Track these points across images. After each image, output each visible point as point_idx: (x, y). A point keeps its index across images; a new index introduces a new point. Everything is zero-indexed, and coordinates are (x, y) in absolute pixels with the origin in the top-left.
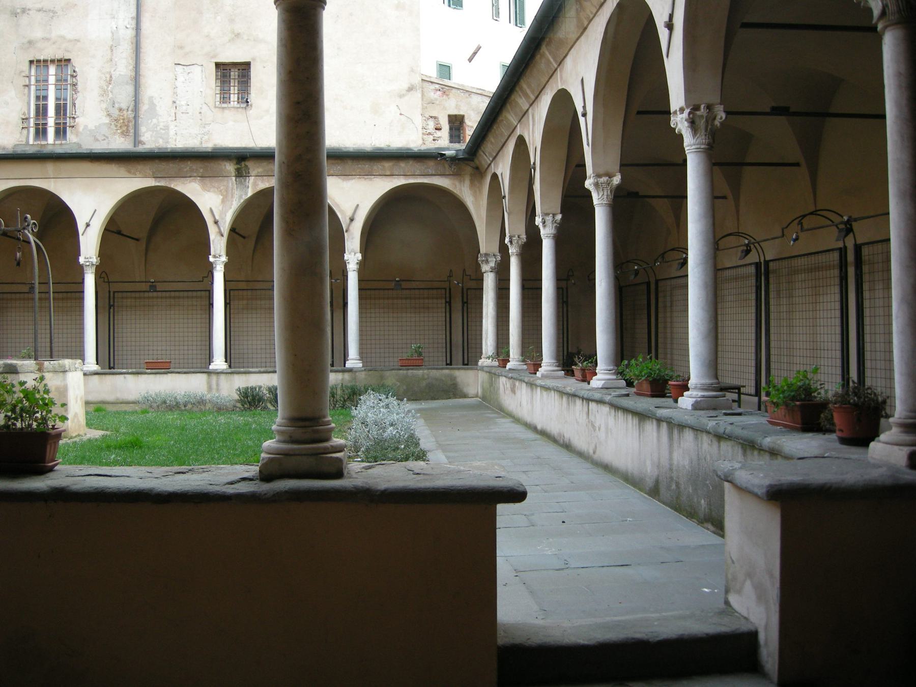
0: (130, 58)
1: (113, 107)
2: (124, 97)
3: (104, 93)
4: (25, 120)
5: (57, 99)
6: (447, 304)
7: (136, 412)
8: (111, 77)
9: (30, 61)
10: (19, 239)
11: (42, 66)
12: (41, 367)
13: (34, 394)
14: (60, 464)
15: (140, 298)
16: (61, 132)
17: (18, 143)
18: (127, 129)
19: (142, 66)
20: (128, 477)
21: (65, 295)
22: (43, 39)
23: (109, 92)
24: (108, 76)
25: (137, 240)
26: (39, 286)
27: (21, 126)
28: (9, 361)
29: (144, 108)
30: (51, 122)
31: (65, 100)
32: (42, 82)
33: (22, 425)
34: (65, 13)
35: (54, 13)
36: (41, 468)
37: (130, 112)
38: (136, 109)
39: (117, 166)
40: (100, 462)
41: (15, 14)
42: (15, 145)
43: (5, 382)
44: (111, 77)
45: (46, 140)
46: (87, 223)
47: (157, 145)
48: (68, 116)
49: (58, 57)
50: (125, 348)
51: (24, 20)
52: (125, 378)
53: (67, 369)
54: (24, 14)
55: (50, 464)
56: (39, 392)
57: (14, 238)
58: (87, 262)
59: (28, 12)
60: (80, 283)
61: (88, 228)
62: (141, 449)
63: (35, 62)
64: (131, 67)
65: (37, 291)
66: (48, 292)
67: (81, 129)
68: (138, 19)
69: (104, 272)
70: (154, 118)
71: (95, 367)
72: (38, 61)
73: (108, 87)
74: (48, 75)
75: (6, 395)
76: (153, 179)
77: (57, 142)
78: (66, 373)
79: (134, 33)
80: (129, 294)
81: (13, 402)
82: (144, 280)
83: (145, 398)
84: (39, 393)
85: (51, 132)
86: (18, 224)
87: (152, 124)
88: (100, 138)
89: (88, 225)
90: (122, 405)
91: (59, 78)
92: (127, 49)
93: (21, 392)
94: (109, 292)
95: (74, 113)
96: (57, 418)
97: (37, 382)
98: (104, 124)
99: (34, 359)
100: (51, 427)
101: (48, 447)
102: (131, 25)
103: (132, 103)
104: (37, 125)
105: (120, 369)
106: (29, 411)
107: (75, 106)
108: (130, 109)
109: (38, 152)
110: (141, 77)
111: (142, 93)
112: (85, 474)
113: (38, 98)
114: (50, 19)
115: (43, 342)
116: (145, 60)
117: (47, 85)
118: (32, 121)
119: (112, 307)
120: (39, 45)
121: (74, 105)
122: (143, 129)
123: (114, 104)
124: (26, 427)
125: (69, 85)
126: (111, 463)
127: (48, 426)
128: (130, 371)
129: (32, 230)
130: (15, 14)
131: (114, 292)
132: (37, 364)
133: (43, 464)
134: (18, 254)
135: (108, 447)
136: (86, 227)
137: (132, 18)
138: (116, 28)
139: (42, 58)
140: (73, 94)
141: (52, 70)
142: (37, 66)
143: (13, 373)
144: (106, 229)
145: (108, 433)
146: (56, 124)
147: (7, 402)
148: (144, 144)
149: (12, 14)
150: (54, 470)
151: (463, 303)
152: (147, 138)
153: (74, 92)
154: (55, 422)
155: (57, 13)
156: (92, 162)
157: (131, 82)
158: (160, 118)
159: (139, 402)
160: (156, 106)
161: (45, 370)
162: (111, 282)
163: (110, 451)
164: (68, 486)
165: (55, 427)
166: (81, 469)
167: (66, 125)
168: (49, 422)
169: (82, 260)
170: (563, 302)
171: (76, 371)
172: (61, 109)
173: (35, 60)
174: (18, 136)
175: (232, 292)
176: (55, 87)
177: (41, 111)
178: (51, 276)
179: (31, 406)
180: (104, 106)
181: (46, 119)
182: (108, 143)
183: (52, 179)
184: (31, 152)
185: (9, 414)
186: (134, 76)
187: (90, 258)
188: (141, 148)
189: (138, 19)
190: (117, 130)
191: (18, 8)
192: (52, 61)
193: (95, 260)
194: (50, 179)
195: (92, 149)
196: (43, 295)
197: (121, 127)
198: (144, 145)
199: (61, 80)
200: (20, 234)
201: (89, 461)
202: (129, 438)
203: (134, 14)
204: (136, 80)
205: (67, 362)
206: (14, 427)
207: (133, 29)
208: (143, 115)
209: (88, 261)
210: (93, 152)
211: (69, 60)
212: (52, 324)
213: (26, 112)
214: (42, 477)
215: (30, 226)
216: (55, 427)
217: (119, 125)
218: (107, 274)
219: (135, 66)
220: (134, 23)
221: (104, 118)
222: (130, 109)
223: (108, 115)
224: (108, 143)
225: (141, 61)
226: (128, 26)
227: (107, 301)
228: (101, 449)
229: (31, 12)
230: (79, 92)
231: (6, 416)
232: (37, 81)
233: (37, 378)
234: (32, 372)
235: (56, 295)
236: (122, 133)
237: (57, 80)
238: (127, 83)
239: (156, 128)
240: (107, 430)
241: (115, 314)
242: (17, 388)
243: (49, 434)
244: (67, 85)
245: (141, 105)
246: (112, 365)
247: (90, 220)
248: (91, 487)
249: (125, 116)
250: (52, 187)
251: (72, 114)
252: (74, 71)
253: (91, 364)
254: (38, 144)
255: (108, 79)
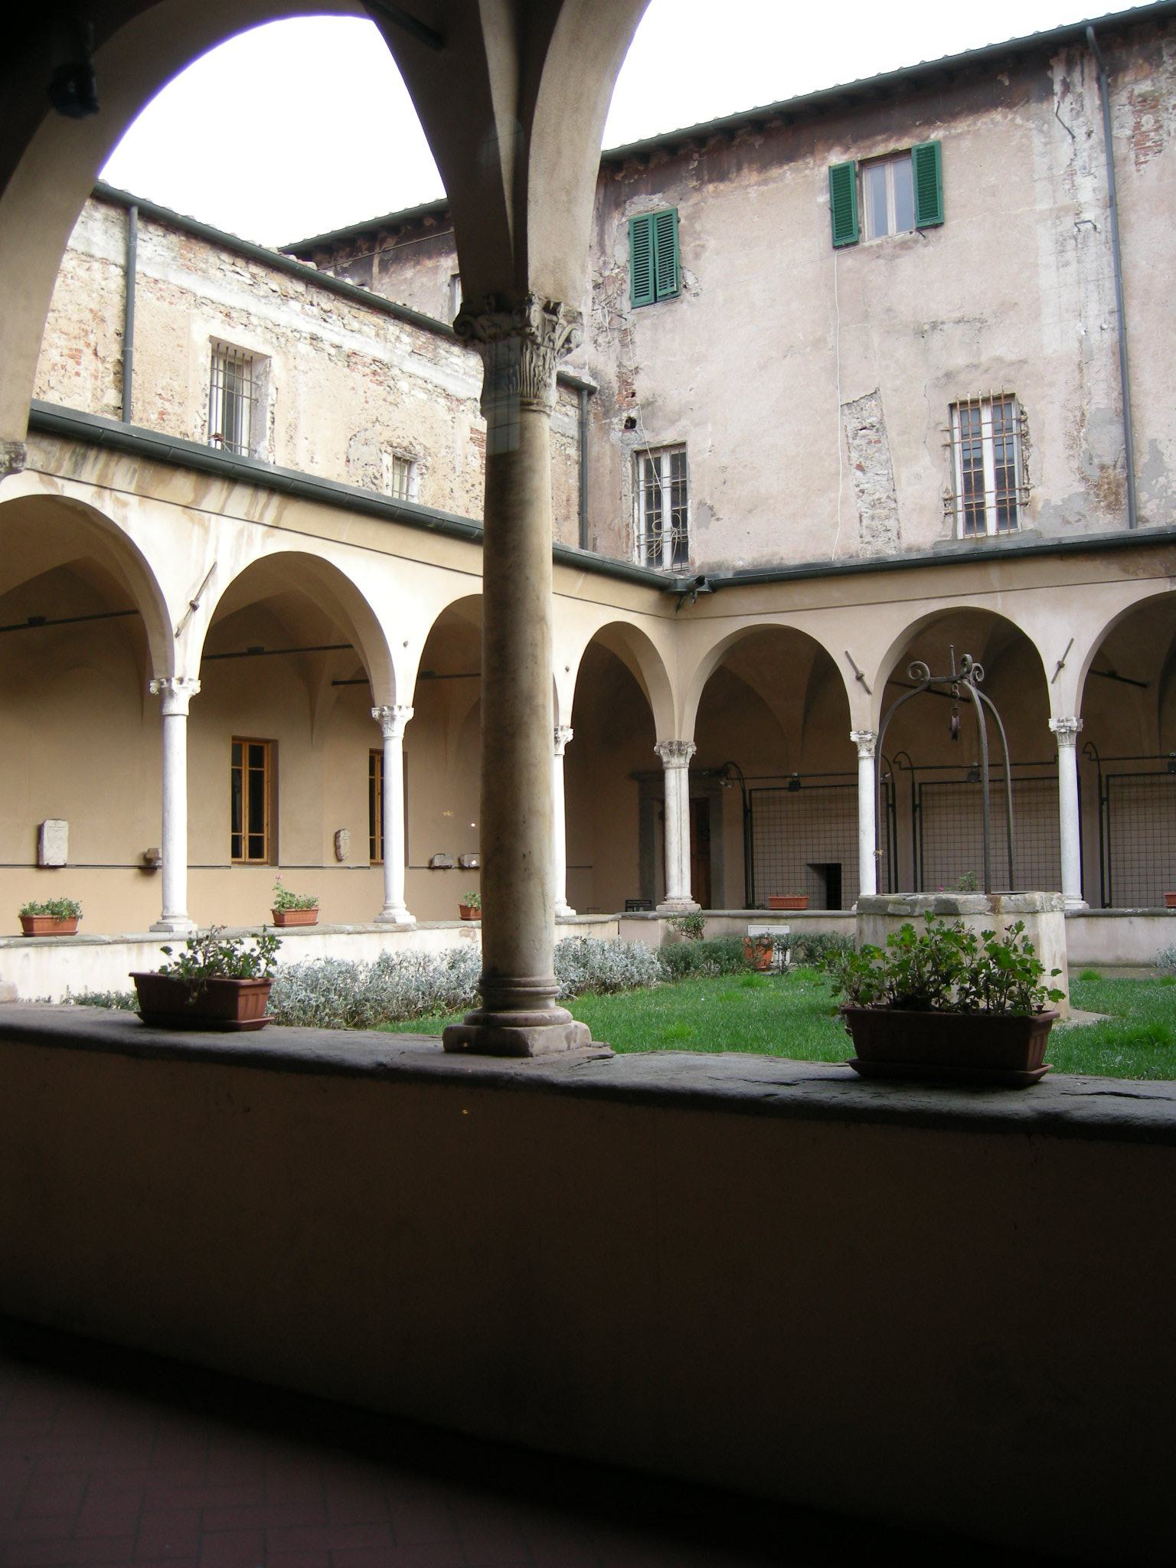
0: (1112, 380)
1: (1091, 464)
2: (1107, 444)
3: (1073, 442)
4: (949, 500)
5: (998, 461)
6: (890, 809)
7: (1152, 982)
8: (1083, 414)
9: (950, 405)
10: (953, 696)
11: (970, 411)
12: (995, 906)
13: (1007, 954)
14: (1049, 1073)
15: (1152, 785)
16: (1006, 514)
17: (939, 539)
18: (1117, 500)
19: (1134, 389)
20: (1169, 1099)
21: (1026, 783)
22: (968, 366)
23: (1082, 440)
24: (1078, 414)
25: (1143, 685)
26: (989, 770)
27: (944, 512)
28: (944, 896)
29: (1143, 459)
30: (990, 499)
31: (1011, 461)
32: (972, 436)
33: (988, 1005)
34: (999, 320)
35: (982, 323)
36: (1022, 1081)
37: (1118, 470)
38: (1129, 463)
39: (1105, 562)
40: (1098, 1068)
41: (922, 334)
42: (936, 543)
43: (960, 932)
44: (1083, 414)
45: (985, 530)
46: (1059, 663)
47: (1169, 520)
48: (1017, 486)
49: (994, 392)
50: (1128, 872)
51: (936, 340)
52: (1131, 922)
53: (1038, 908)
54: (935, 331)
55: (1035, 1072)
56: (1016, 949)
57: (946, 695)
58: (1062, 727)
59: (941, 326)
60: (1050, 763)
61: (1062, 669)
62: (1167, 1047)
63: (958, 406)
64: (1115, 394)
65: (986, 779)
66: (1002, 780)
67: (1039, 507)
68: (1121, 312)
69: (1091, 743)
70: (1160, 476)
71: (1079, 905)
72: (964, 403)
73: (1079, 432)
74: (980, 424)
75: (962, 954)
76: (1168, 580)
77: (1002, 532)
78: (1038, 915)
79: (1116, 336)
80: (1133, 779)
81: (973, 966)
82: (1158, 754)
83: (1168, 957)
84: (1017, 951)
85: (991, 515)
86: (952, 671)
87: (1158, 486)
88: (1072, 519)
89: (1061, 665)
90: (1127, 969)
91: (998, 426)
92: (1106, 365)
93: (986, 949)
94: (1100, 776)
95: (1026, 481)
96: (1046, 994)
97: (1011, 934)
98: (1077, 494)
99: (983, 892)
100: (1036, 1009)
101: (1032, 1042)
102: (1110, 323)
103: (1122, 455)
104: (968, 506)
105: (1121, 907)
106: (1000, 981)
107: (1027, 469)
108: (1119, 464)
109: (974, 550)
110: (1134, 409)
111: (1136, 435)
112: (1094, 1092)
113: (966, 463)
114: (977, 332)
115: (998, 863)
116: (1137, 379)
117: (981, 441)
118: (960, 500)
119: (1105, 803)
120: (962, 377)
121: (1026, 467)
122: (1143, 496)
123: (1091, 458)
124: (995, 1009)
125: (1015, 437)
126: (1115, 1069)
127: (1030, 1007)
128: (1140, 910)
129: (975, 679)
130: (922, 334)
131: (1108, 777)
132: (989, 900)
133: (1023, 1072)
134: (954, 720)
135: (1110, 1042)
136: (1059, 670)
137: (1111, 312)
138: (1085, 331)
139: (968, 398)
140: (1022, 451)
141: (986, 415)
142: (961, 412)
143: (950, 915)
144: (1090, 671)
145: (1108, 1017)
146: (999, 502)
147: (965, 966)
148: (1147, 521)
149: (915, 334)
150: (1040, 1083)
151: (914, 808)
152: (1152, 511)
153: (1024, 447)
154: (1042, 1000)
155: (986, 322)
156: (1062, 560)
157: (1116, 418)
158: (1170, 474)
159: (1156, 964)
160: (1163, 454)
161: (1002, 910)
162: (1104, 760)
163: (1112, 1049)
164: (1067, 1112)
165: (1043, 1009)
166: (1085, 1081)
167: (1015, 502)
168: (1032, 1001)
169: (1053, 724)
170: (888, 805)
171: (1053, 911)
172: (1004, 478)
173: (958, 403)
174: (940, 525)
175: (1112, 781)
176: (994, 441)
177: (974, 484)
178: (1007, 753)
179: (1002, 974)
180: (1075, 464)
181: (982, 496)
182: (1086, 526)
183: (999, 593)
184: (961, 552)
185: (967, 985)
186: (1122, 408)
187: (1067, 721)
188: (1142, 529)
189: (1121, 312)
190: (1100, 501)
191: (925, 323)
192: (986, 401)
193: (1075, 723)
194: (995, 594)
195: (1060, 539)
196: (998, 785)
197: (1105, 496)
198: (1146, 524)
199: (1002, 430)
200: (956, 688)
201: (1078, 1064)
202: (1144, 1028)
203: (1114, 305)
204: (1126, 415)
205: (1038, 897)
206: (974, 1007)
207: (1113, 329)
208: (1142, 473)
209: (1064, 726)
210: (1063, 542)
211: (1012, 396)
212: (1012, 831)
213: (950, 488)
214: (1022, 1093)
215: (971, 674)
216: (1043, 1009)
217: (1102, 494)
218: (1094, 748)
219: (1121, 392)
220: (1114, 320)
221: (1076, 484)
222: (1119, 464)
223: (1083, 478)
224: (1086, 526)
225: (1132, 382)
226: (1105, 326)
227: (1097, 791)
228: (1097, 1045)
229: (945, 327)
230: (1032, 446)
231: (962, 989)
232: (964, 436)
233: (1011, 926)
234: (980, 914)
235: (1019, 784)
236: (1109, 507)
237: (995, 431)
238: (1111, 422)
239: (1166, 491)
240: (1105, 1012)
241: (1111, 814)
242: (981, 944)
243: (1033, 1021)
244: (1012, 436)
245: (1137, 456)
246: (1107, 901)
247: (1064, 658)
248: (1106, 1115)
249: (1112, 477)
250: (1000, 606)
251: (1024, 483)
252: (1022, 413)
253: (1072, 896)
254: (972, 538)
255: (1078, 419)
